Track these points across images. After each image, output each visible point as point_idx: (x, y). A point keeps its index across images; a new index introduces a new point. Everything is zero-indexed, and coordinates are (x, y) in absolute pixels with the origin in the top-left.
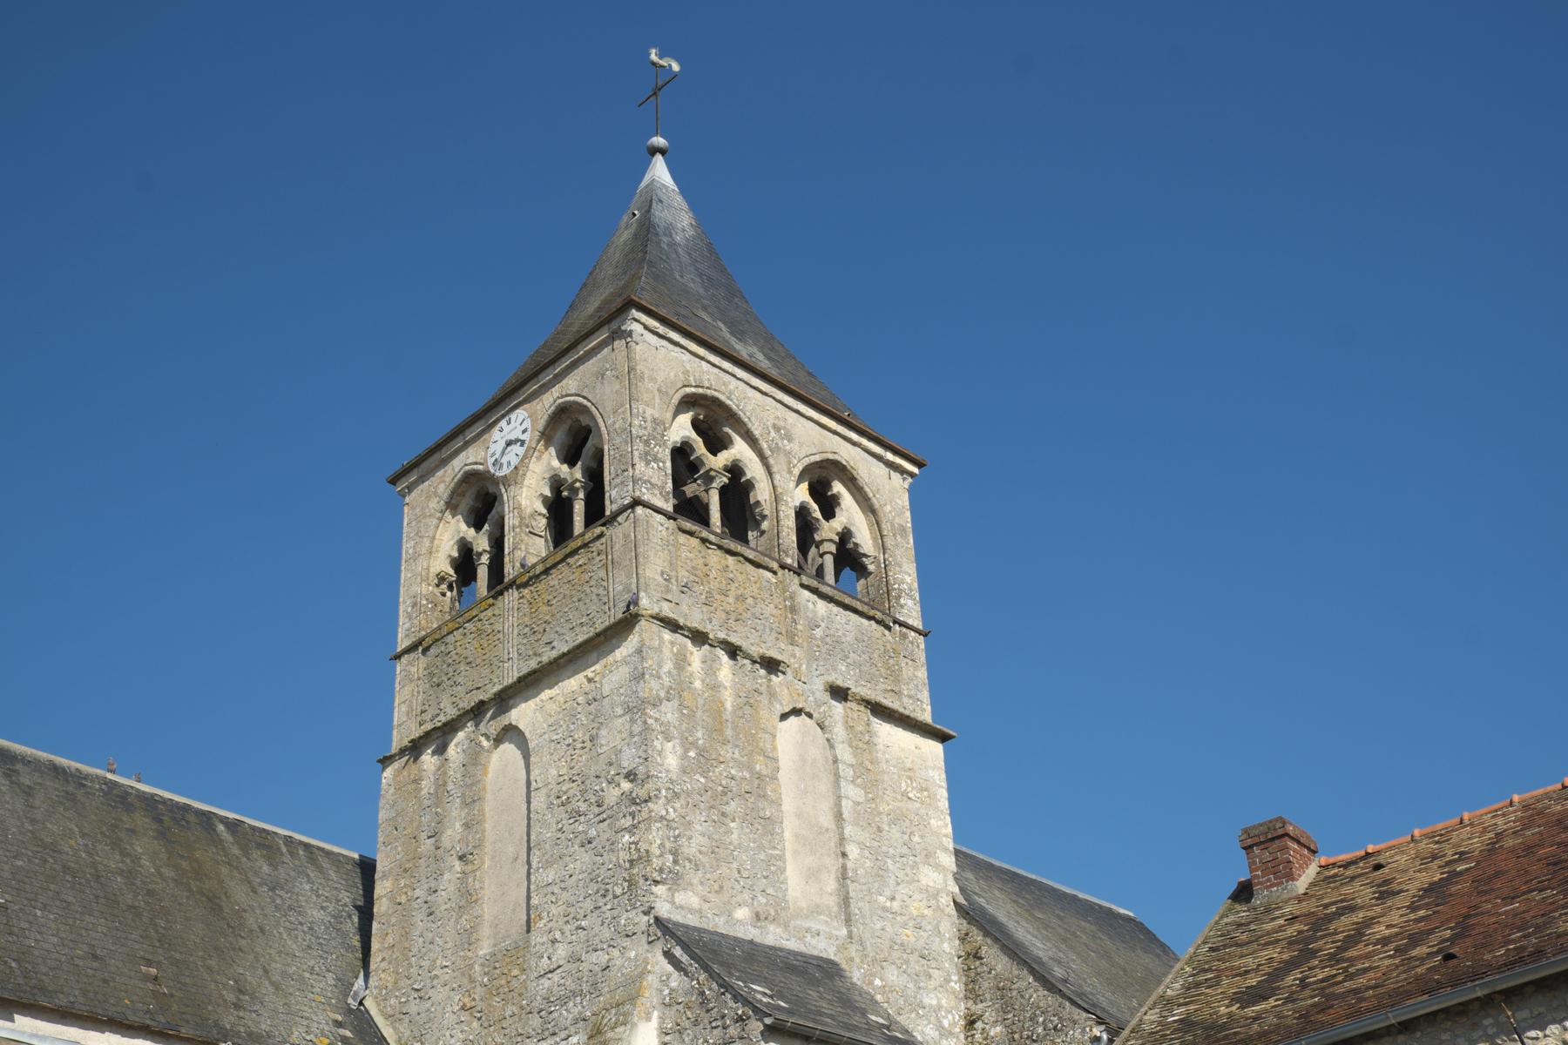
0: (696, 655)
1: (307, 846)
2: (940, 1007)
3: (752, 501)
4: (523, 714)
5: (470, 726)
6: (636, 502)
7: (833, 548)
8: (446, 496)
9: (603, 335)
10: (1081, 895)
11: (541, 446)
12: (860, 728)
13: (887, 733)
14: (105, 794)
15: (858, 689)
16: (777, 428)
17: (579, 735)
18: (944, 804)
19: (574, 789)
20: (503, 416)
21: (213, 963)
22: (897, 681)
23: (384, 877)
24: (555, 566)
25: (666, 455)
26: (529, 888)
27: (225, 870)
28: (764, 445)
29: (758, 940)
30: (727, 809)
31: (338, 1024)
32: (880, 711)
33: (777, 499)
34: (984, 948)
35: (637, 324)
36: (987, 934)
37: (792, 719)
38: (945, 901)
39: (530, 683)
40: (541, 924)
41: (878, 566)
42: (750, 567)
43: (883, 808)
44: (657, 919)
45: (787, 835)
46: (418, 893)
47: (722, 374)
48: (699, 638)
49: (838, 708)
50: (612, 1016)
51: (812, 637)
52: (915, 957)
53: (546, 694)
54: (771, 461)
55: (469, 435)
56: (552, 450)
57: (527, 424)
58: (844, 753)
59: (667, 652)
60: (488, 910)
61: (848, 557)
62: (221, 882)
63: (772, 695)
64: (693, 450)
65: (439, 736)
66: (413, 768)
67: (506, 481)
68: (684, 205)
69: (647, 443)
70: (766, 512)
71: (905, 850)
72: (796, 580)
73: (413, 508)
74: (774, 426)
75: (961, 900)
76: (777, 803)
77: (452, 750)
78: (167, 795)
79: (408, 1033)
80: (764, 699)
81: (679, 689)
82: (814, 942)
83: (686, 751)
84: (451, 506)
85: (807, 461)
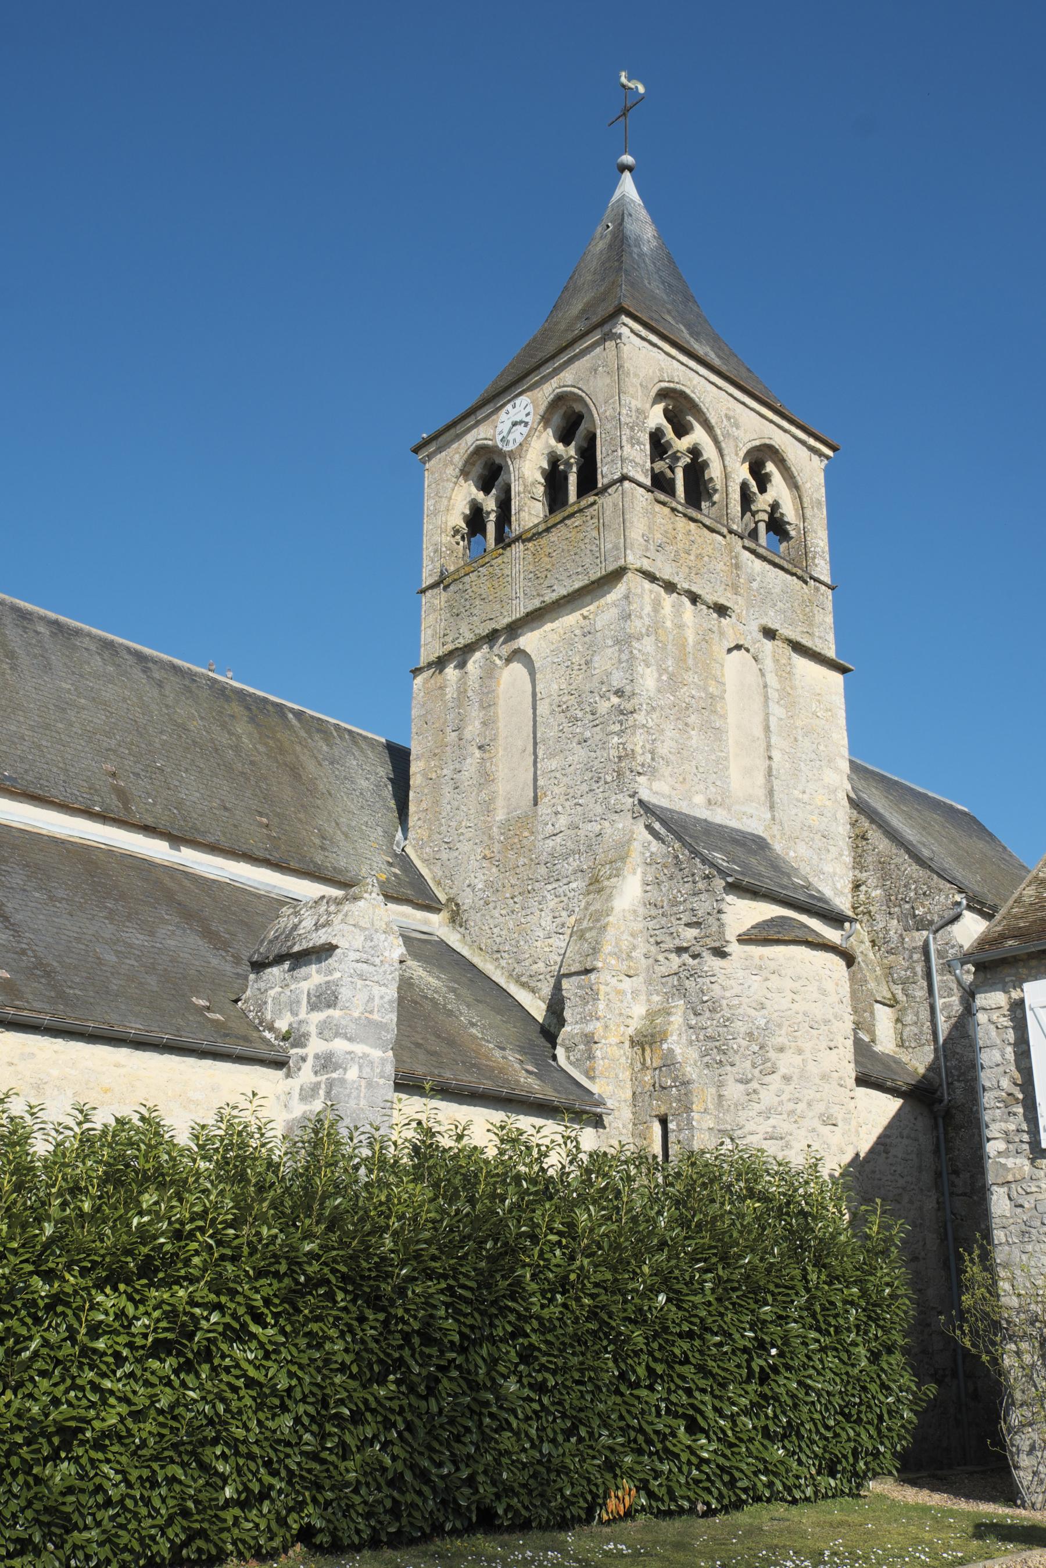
0: (669, 601)
1: (350, 732)
2: (835, 874)
3: (707, 477)
4: (529, 641)
5: (485, 648)
6: (624, 478)
7: (766, 517)
8: (460, 465)
9: (596, 336)
10: (930, 794)
11: (540, 427)
12: (784, 661)
13: (803, 665)
14: (211, 688)
15: (785, 631)
16: (728, 418)
17: (576, 659)
18: (842, 722)
19: (572, 701)
20: (509, 401)
21: (301, 816)
22: (811, 625)
23: (418, 758)
24: (555, 525)
25: (645, 438)
26: (535, 773)
27: (298, 748)
28: (718, 432)
29: (710, 819)
30: (690, 720)
31: (390, 864)
32: (798, 648)
33: (726, 477)
34: (870, 832)
35: (625, 327)
36: (872, 821)
37: (735, 652)
38: (842, 796)
39: (535, 617)
40: (546, 800)
41: (799, 532)
42: (706, 532)
43: (799, 723)
44: (640, 801)
45: (730, 741)
46: (445, 772)
47: (688, 371)
48: (670, 587)
49: (768, 645)
50: (606, 870)
51: (750, 588)
52: (818, 837)
53: (548, 627)
54: (723, 445)
55: (480, 415)
56: (550, 431)
57: (530, 408)
58: (772, 680)
59: (647, 599)
60: (502, 787)
61: (777, 526)
62: (297, 757)
63: (722, 633)
64: (663, 434)
65: (461, 655)
66: (439, 678)
67: (511, 454)
68: (648, 219)
69: (632, 429)
70: (718, 487)
71: (813, 756)
72: (740, 542)
73: (433, 473)
74: (726, 416)
75: (853, 795)
76: (724, 717)
77: (470, 666)
78: (251, 690)
79: (440, 873)
80: (716, 637)
81: (655, 628)
82: (748, 822)
83: (660, 675)
84: (465, 473)
85: (749, 446)
